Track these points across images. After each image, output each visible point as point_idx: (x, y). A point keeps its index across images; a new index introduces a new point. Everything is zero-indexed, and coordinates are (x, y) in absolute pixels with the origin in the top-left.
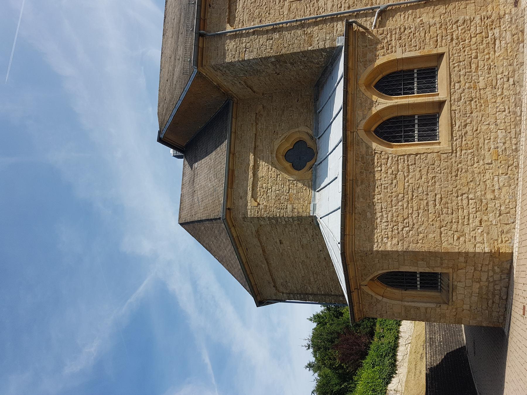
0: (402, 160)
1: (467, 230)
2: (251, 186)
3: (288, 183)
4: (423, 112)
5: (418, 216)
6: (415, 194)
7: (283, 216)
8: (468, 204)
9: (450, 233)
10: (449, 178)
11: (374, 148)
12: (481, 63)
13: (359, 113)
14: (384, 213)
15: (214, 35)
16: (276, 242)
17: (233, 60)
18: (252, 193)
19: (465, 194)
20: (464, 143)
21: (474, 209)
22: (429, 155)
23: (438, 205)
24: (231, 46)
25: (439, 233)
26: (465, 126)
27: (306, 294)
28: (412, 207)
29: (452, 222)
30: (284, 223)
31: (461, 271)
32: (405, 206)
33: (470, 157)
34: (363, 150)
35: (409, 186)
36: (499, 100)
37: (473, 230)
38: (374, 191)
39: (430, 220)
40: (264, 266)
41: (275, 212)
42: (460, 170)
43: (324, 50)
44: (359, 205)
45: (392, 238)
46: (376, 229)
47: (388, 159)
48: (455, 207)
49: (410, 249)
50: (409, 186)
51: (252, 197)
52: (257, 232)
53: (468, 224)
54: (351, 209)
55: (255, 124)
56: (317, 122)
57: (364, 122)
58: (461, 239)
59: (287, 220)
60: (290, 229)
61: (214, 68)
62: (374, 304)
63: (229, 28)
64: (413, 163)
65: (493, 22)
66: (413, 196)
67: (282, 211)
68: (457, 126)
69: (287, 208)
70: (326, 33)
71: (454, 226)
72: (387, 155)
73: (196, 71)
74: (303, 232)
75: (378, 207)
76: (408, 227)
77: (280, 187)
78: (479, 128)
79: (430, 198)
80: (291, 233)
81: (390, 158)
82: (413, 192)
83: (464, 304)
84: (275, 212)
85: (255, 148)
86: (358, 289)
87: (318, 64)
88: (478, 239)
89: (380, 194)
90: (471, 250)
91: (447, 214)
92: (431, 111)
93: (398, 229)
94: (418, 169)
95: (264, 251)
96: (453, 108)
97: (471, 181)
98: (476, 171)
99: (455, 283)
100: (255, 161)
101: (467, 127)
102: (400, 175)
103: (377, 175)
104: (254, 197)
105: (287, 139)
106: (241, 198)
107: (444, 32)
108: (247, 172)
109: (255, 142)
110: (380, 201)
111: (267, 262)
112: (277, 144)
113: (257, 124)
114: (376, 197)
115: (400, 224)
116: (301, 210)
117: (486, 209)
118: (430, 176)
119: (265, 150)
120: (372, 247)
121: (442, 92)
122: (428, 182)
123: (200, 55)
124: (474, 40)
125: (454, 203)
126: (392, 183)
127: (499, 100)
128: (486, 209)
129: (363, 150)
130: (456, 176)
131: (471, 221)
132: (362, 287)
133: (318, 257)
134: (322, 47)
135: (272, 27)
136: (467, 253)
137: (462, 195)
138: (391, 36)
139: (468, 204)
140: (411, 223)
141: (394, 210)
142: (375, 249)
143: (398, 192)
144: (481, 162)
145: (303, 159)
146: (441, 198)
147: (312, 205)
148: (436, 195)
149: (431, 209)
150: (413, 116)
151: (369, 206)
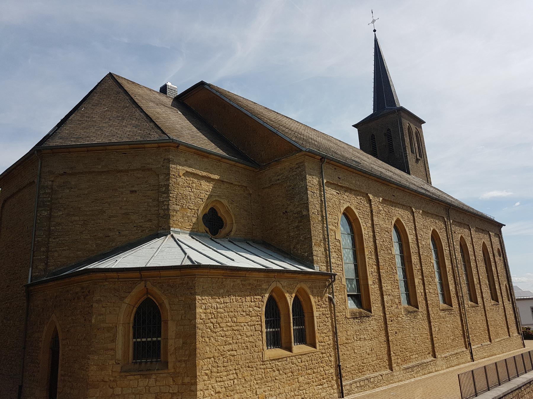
0: (258, 320)
1: (213, 381)
2: (195, 172)
3: (196, 208)
4: (283, 335)
5: (222, 336)
6: (236, 332)
7: (170, 200)
8: (230, 380)
9: (210, 366)
10: (247, 361)
11: (266, 295)
12: (311, 377)
13: (285, 283)
14: (223, 305)
15: (322, 169)
16: (133, 187)
17: (308, 181)
18: (189, 172)
19: (237, 375)
20: (268, 370)
21: (227, 386)
22: (261, 342)
23: (229, 353)
24: (315, 181)
25: (210, 356)
26: (278, 370)
27: (51, 209)
28: (227, 331)
29: (218, 367)
30: (161, 199)
31: (172, 381)
32: (229, 324)
33: (260, 376)
34: (264, 286)
35: (242, 326)
36: (293, 394)
37: (212, 387)
38: (238, 296)
39: (219, 347)
40: (100, 167)
41: (173, 192)
42: (252, 369)
43: (311, 254)
44: (229, 282)
45: (205, 313)
46: (212, 298)
47: (259, 307)
48: (228, 368)
49: (198, 331)
50: (242, 326)
51: (187, 172)
52: (150, 170)
53: (217, 382)
54: (226, 275)
55: (240, 184)
56: (239, 241)
57: (281, 287)
58: (206, 377)
59: (165, 203)
60: (150, 204)
61: (300, 163)
62: (116, 294)
63: (325, 181)
64: (257, 329)
65: (330, 382)
66: (235, 331)
67: (174, 200)
68: (278, 363)
69: (177, 205)
70: (321, 257)
71: (215, 370)
72: (255, 306)
73: (304, 149)
74: (146, 216)
75: (227, 300)
76: (214, 328)
77: (193, 200)
78: (277, 381)
79: (235, 346)
80: (146, 204)
81: (259, 309)
82: (238, 330)
83: (122, 388)
84: (173, 192)
85: (223, 181)
86: (141, 278)
87: (294, 248)
88: (206, 392)
89: (236, 301)
90: (199, 387)
91: (224, 362)
92: (283, 341)
93: (212, 318)
94: (252, 334)
95: (121, 171)
96: (288, 359)
97: (245, 380)
98: (252, 383)
99: (154, 377)
100: (213, 180)
101: (277, 372)
102: (248, 318)
103: (248, 298)
104: (187, 174)
105: (228, 212)
106: (186, 161)
107: (326, 347)
108: (206, 170)
109: (227, 182)
110: (231, 301)
111: (105, 172)
112: (225, 202)
113: (239, 186)
114: (234, 298)
115: (215, 320)
116: (175, 218)
117: (227, 396)
118: (248, 344)
119: (221, 190)
120: (199, 295)
121: (298, 348)
122: (244, 343)
123: (311, 154)
124: (322, 369)
125: (231, 368)
126: (243, 312)
127: (293, 394)
128: (227, 396)
129: (264, 286)
130: (249, 367)
131: (219, 383)
132: (143, 283)
133: (110, 230)
134: (314, 254)
135: (324, 215)
136: (195, 384)
137: (236, 374)
138: (324, 308)
139: (230, 380)
140: (217, 330)
141: (225, 314)
142: (198, 297)
143: (238, 318)
144: (257, 386)
145: (212, 226)
146: (234, 355)
147: (179, 230)
148: (236, 351)
149: (227, 347)
150: (279, 326)
151: (228, 291)
